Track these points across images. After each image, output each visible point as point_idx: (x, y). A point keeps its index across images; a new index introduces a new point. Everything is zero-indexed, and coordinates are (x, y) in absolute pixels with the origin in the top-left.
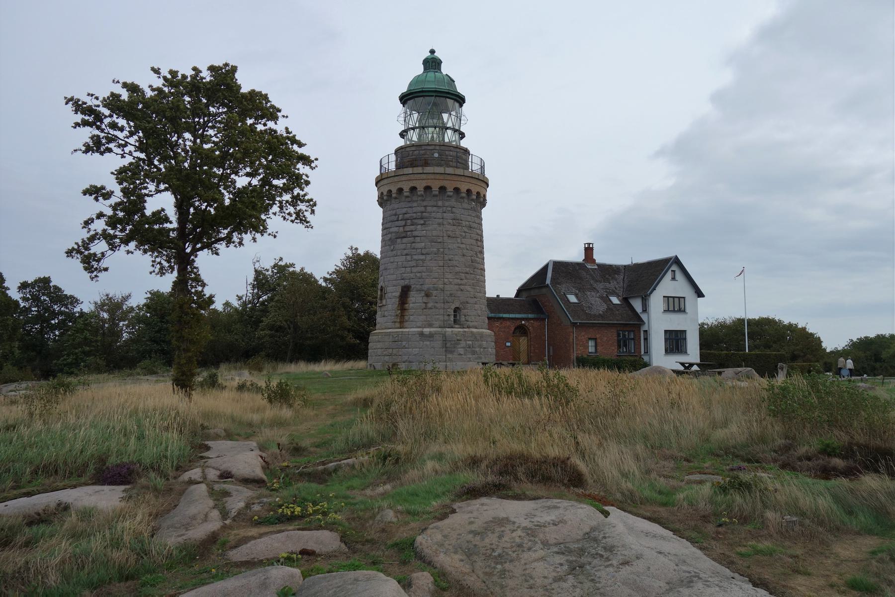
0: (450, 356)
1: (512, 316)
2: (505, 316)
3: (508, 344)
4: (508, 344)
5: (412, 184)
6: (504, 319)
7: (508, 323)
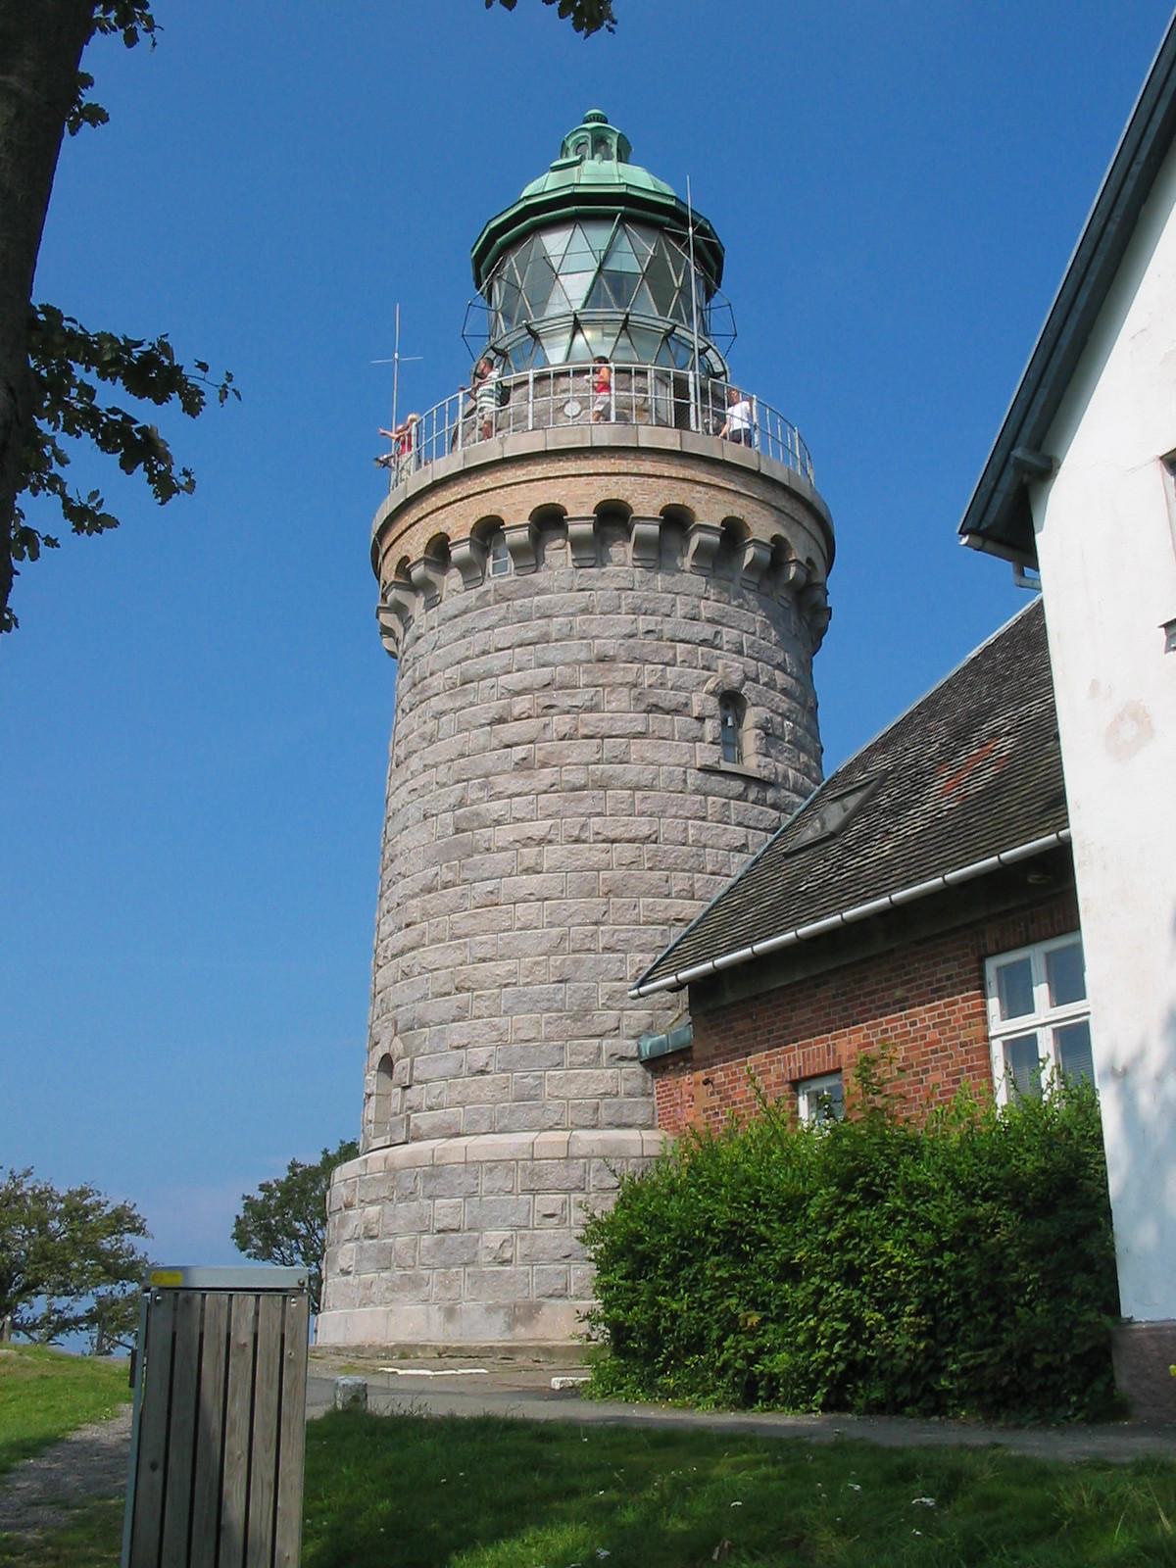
5: (679, 495)
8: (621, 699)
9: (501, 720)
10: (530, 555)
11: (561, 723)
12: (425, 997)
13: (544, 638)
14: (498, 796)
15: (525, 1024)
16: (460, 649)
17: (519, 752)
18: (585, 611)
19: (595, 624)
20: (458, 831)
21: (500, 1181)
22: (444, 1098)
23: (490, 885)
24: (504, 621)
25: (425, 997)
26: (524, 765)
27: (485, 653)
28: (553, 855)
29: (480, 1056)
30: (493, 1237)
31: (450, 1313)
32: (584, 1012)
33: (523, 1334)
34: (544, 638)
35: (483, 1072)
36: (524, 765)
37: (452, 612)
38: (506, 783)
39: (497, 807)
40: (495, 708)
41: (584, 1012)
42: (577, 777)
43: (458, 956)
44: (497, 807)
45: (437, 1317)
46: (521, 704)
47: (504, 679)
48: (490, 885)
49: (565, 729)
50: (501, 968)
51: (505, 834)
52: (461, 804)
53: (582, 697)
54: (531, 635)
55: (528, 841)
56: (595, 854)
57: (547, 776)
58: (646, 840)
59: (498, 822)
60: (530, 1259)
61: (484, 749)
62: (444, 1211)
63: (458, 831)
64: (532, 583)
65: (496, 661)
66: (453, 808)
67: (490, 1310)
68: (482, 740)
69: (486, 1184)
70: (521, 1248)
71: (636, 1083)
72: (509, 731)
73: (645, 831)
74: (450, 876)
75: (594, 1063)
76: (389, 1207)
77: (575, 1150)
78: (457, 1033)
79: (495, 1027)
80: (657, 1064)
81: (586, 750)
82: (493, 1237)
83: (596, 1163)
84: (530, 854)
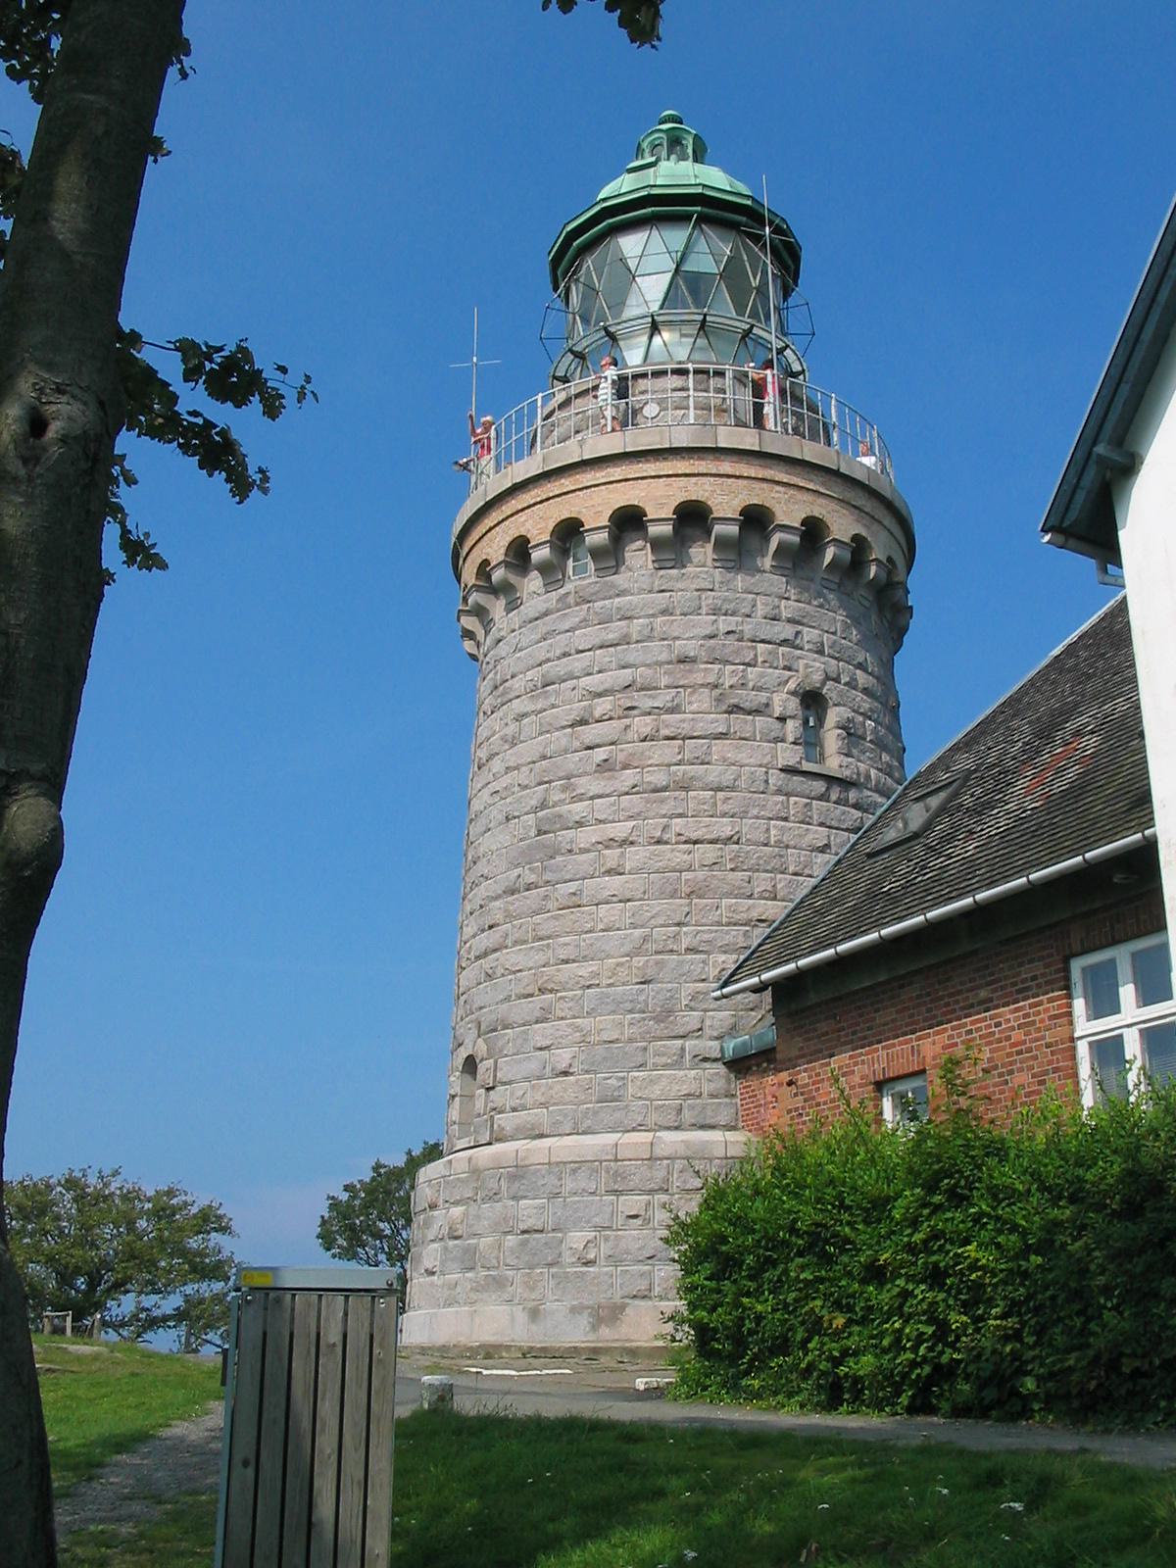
5: (819, 509)
8: (703, 700)
9: (583, 722)
10: (610, 557)
11: (642, 725)
12: (508, 999)
13: (625, 640)
14: (580, 798)
15: (607, 1026)
16: (541, 651)
17: (600, 754)
18: (664, 612)
19: (676, 625)
20: (540, 833)
21: (583, 1182)
22: (529, 1100)
23: (572, 887)
24: (584, 623)
25: (508, 999)
26: (605, 767)
27: (565, 655)
28: (635, 856)
29: (563, 1057)
30: (577, 1238)
31: (534, 1314)
32: (666, 1014)
33: (607, 1335)
34: (625, 640)
35: (566, 1073)
36: (605, 767)
37: (533, 614)
38: (589, 785)
39: (579, 809)
40: (576, 709)
41: (666, 1014)
42: (659, 778)
43: (540, 958)
44: (579, 809)
45: (522, 1317)
46: (603, 706)
47: (585, 681)
48: (572, 887)
49: (646, 731)
50: (584, 970)
51: (587, 836)
52: (543, 806)
53: (663, 699)
54: (612, 636)
55: (610, 843)
56: (678, 855)
57: (629, 777)
58: (728, 840)
59: (580, 824)
60: (614, 1260)
61: (566, 751)
62: (529, 1210)
63: (540, 833)
64: (613, 585)
65: (577, 663)
66: (535, 810)
67: (574, 1310)
68: (564, 742)
69: (569, 1185)
70: (605, 1249)
71: (720, 1084)
72: (590, 733)
73: (728, 831)
74: (533, 878)
75: (678, 1064)
76: (473, 1209)
77: (658, 1152)
78: (541, 1034)
79: (578, 1029)
80: (741, 1065)
81: (666, 751)
82: (577, 1238)
83: (679, 1164)
84: (611, 856)
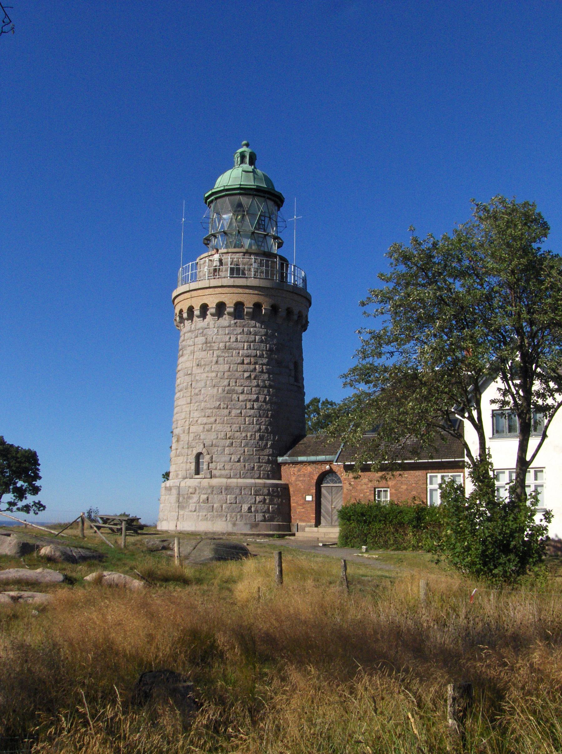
0: (181, 512)
1: (313, 458)
2: (301, 459)
3: (309, 498)
4: (309, 498)
5: (240, 298)
6: (301, 463)
7: (309, 468)
31: (234, 525)
45: (230, 525)
67: (246, 524)
